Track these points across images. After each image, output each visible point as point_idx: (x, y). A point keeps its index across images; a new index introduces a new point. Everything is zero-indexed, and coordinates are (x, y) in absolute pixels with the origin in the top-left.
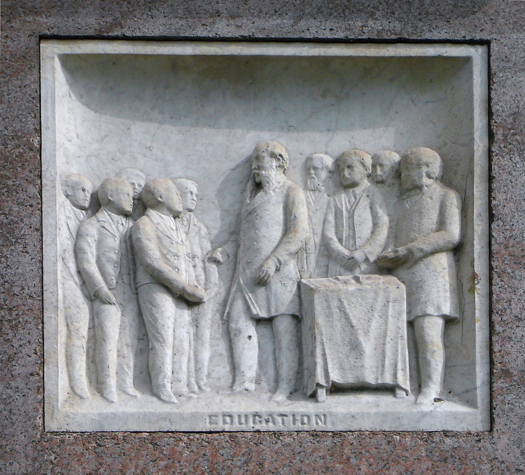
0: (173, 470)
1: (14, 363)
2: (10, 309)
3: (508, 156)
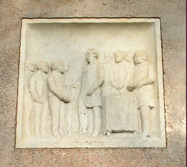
0: (58, 162)
1: (7, 124)
2: (7, 105)
3: (168, 53)
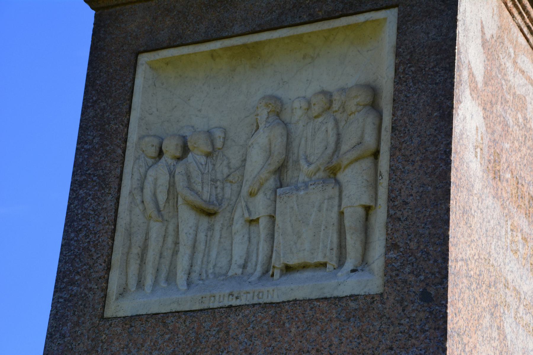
3: (405, 84)
